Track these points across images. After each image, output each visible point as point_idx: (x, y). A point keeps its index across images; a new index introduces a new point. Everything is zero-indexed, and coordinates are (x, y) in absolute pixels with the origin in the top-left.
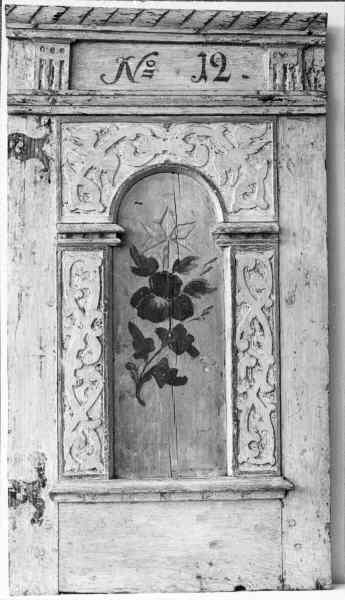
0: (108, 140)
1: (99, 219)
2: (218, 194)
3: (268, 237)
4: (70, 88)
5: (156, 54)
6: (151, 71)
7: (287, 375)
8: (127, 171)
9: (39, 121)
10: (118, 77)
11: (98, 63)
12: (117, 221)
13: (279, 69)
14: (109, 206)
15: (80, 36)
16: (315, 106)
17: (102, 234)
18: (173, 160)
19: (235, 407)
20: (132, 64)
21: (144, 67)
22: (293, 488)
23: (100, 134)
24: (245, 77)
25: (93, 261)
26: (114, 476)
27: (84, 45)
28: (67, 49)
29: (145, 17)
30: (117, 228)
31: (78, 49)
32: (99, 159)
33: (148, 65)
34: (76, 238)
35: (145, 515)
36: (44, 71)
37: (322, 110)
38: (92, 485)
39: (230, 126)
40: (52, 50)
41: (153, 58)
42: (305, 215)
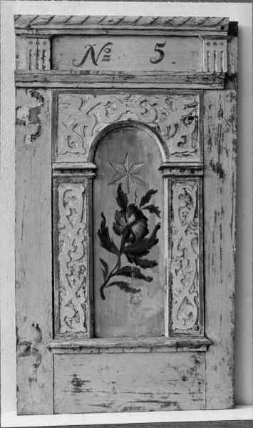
0: (86, 108)
1: (83, 161)
4: (52, 67)
9: (26, 91)
10: (83, 61)
11: (71, 50)
12: (93, 162)
16: (23, 82)
17: (81, 170)
20: (97, 50)
21: (103, 53)
22: (212, 343)
26: (94, 336)
28: (48, 42)
30: (92, 166)
31: (56, 43)
32: (83, 120)
36: (223, 61)
40: (37, 43)
41: (109, 46)
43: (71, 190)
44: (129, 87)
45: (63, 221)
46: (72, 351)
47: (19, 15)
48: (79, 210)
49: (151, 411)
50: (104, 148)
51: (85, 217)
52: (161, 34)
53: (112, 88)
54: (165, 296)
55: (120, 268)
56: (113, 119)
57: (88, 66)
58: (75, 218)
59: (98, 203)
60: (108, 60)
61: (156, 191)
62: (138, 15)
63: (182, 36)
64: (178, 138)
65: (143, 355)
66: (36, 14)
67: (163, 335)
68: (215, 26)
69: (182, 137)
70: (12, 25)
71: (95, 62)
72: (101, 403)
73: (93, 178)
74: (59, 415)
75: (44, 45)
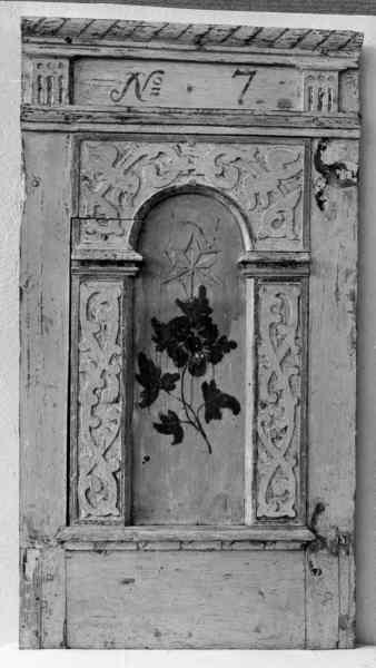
1: (121, 247)
2: (245, 219)
3: (290, 270)
5: (162, 72)
8: (148, 193)
12: (137, 251)
17: (121, 263)
18: (200, 181)
20: (142, 79)
23: (119, 156)
25: (111, 291)
26: (130, 522)
27: (87, 63)
28: (66, 63)
29: (308, 39)
30: (139, 257)
37: (356, 134)
38: (150, 533)
39: (261, 147)
42: (337, 240)
44: (132, 130)
45: (86, 340)
46: (251, 547)
47: (65, 20)
49: (147, 648)
50: (150, 235)
52: (214, 60)
53: (79, 131)
54: (231, 468)
55: (182, 425)
57: (130, 99)
60: (157, 94)
63: (217, 63)
65: (254, 554)
68: (175, 39)
71: (139, 96)
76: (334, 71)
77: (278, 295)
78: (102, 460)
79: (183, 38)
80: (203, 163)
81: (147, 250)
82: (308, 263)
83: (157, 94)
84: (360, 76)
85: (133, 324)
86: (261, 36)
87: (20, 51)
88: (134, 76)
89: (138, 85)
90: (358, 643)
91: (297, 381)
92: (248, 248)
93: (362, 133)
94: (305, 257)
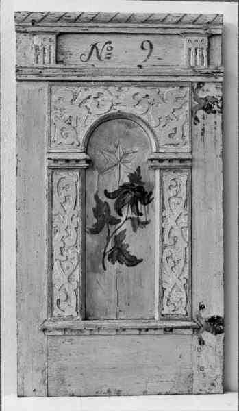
3: (186, 163)
5: (110, 43)
6: (110, 54)
7: (196, 270)
10: (90, 54)
11: (77, 48)
12: (86, 152)
13: (193, 50)
14: (81, 141)
15: (62, 30)
17: (77, 161)
19: (161, 282)
20: (100, 46)
23: (75, 96)
24: (159, 59)
26: (86, 318)
32: (74, 110)
33: (108, 50)
34: (60, 165)
35: (98, 340)
43: (64, 178)
48: (72, 199)
51: (78, 204)
56: (103, 111)
58: (69, 206)
59: (90, 182)
61: (141, 261)
62: (198, 12)
64: (170, 129)
66: (199, 14)
67: (154, 319)
69: (173, 129)
70: (13, 24)
72: (44, 201)
73: (86, 169)
74: (51, 398)
75: (48, 43)
76: (53, 33)
77: (174, 179)
78: (67, 276)
79: (214, 22)
80: (126, 100)
81: (90, 152)
82: (191, 160)
83: (109, 58)
84: (222, 40)
85: (163, 204)
86: (84, 16)
87: (14, 29)
88: (94, 46)
89: (98, 53)
90: (226, 390)
91: (186, 232)
92: (154, 150)
93: (224, 79)
94: (189, 156)
